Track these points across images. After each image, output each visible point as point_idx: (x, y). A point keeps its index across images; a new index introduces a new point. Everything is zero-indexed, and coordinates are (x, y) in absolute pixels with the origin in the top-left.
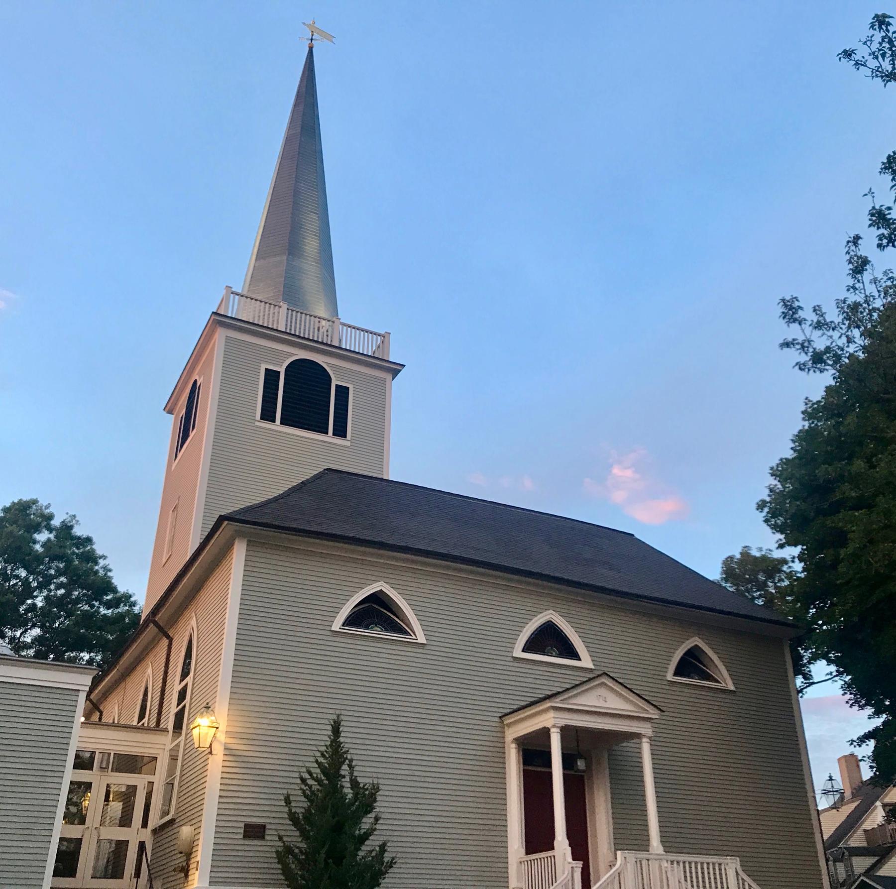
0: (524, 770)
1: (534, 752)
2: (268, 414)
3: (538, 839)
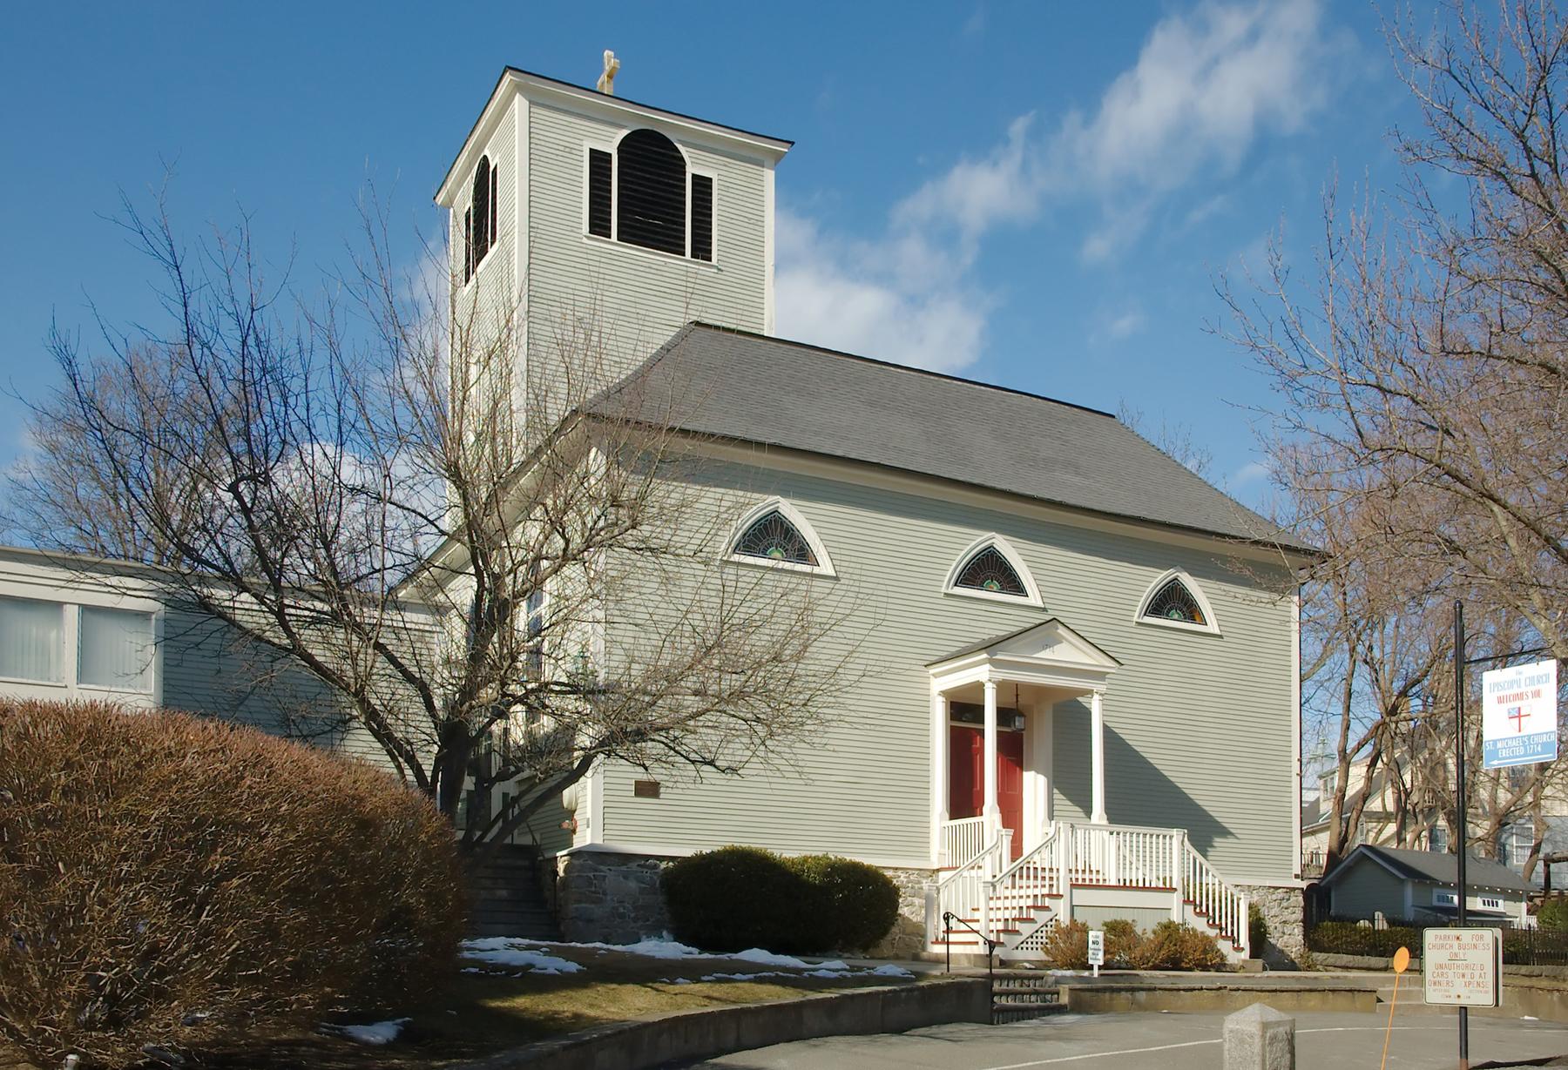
0: (953, 729)
1: (964, 709)
2: (599, 225)
3: (964, 801)
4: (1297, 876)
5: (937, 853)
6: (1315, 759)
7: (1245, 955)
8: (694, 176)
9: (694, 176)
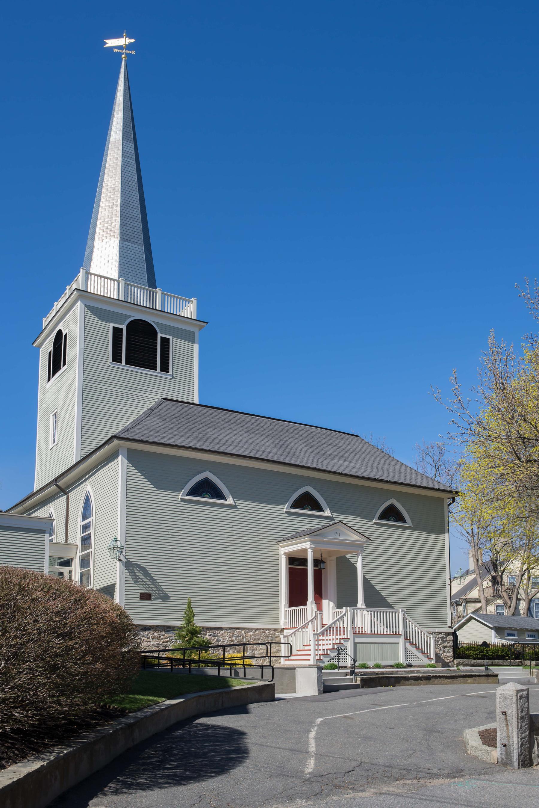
0: (290, 569)
2: (116, 358)
4: (449, 627)
5: (283, 622)
6: (457, 577)
7: (434, 662)
8: (162, 338)
9: (162, 338)
